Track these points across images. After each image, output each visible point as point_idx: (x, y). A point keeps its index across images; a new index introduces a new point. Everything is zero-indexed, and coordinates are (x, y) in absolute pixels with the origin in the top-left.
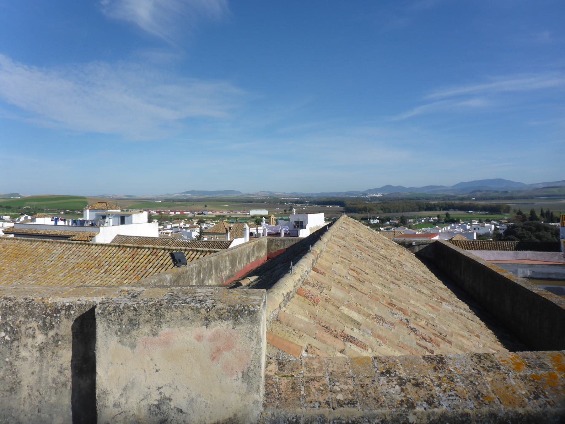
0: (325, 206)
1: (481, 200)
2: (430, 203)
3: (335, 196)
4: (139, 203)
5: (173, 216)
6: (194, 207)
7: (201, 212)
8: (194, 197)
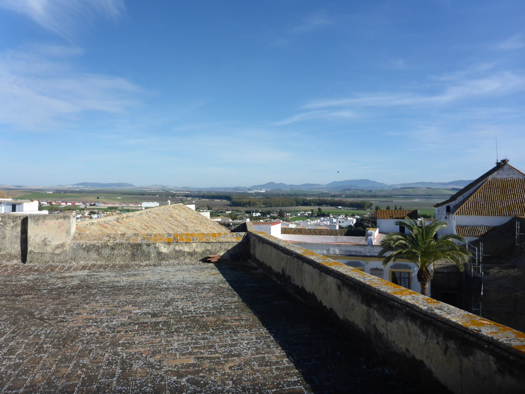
0: (213, 199)
1: (350, 197)
2: (306, 199)
3: (223, 191)
4: (30, 193)
5: (65, 207)
6: (86, 199)
7: (93, 204)
8: (87, 189)
